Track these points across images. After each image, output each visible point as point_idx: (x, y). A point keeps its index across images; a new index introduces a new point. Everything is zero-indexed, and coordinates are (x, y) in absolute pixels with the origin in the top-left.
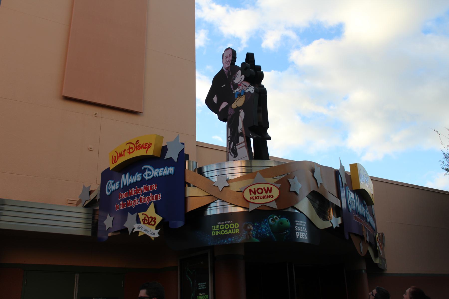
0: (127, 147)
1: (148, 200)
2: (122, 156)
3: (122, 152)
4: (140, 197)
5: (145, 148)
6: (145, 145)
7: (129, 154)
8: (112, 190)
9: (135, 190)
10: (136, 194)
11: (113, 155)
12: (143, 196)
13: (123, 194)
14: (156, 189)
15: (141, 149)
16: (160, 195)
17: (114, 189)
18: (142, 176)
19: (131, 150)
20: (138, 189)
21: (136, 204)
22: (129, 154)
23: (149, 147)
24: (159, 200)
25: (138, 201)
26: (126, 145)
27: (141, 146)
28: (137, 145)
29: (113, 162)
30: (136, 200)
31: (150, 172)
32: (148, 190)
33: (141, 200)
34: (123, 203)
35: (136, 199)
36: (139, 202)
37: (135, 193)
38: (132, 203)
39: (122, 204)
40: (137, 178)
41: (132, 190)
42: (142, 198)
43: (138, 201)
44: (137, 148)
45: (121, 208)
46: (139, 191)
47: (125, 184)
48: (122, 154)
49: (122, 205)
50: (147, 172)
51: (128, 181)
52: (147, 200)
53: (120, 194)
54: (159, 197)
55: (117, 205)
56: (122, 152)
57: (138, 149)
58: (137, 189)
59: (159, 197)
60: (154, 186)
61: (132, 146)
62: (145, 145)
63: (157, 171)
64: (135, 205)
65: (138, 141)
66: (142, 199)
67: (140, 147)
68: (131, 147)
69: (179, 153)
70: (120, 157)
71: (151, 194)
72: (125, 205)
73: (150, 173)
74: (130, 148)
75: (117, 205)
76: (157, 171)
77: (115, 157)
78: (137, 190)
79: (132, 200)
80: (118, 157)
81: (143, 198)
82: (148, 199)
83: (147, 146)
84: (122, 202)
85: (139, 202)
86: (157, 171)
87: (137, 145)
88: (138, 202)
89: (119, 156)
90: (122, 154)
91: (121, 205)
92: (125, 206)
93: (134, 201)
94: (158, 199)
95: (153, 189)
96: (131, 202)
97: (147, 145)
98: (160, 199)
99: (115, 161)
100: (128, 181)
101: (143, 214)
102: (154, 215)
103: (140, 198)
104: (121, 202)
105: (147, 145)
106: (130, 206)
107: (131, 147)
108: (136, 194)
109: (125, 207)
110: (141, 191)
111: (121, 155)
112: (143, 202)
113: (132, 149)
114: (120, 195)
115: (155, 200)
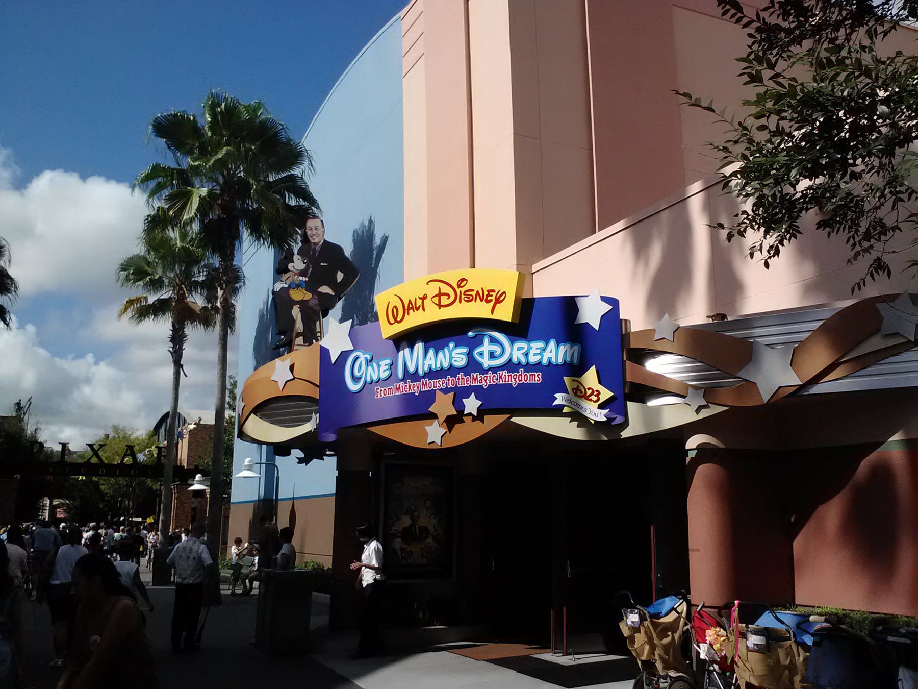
0: (433, 290)
1: (515, 379)
2: (418, 309)
3: (418, 299)
4: (499, 373)
5: (488, 301)
6: (486, 293)
7: (440, 308)
8: (369, 380)
9: (406, 386)
10: (408, 392)
11: (389, 302)
12: (505, 372)
13: (383, 389)
14: (443, 386)
15: (475, 301)
16: (539, 374)
17: (375, 378)
18: (470, 355)
19: (444, 300)
20: (412, 384)
21: (490, 382)
22: (440, 308)
23: (498, 301)
24: (536, 382)
25: (494, 378)
26: (427, 284)
27: (474, 293)
28: (463, 290)
29: (392, 321)
30: (490, 376)
31: (497, 349)
32: (430, 388)
33: (501, 377)
34: (463, 377)
35: (489, 375)
36: (497, 379)
37: (406, 390)
38: (482, 379)
39: (460, 377)
40: (451, 358)
41: (400, 385)
42: (502, 375)
43: (495, 379)
44: (463, 296)
45: (459, 384)
46: (413, 388)
47: (411, 369)
48: (417, 306)
49: (460, 380)
50: (487, 347)
51: (424, 364)
52: (513, 380)
53: (377, 389)
54: (537, 378)
55: (451, 379)
56: (418, 299)
57: (466, 299)
58: (410, 384)
59: (537, 378)
60: (441, 383)
61: (445, 289)
62: (486, 293)
63: (523, 348)
64: (488, 383)
65: (463, 280)
66: (503, 376)
67: (472, 295)
68: (442, 292)
69: (602, 316)
70: (411, 311)
71: (521, 371)
72: (467, 381)
73: (496, 351)
74: (440, 295)
75: (451, 379)
76: (523, 348)
77: (395, 309)
78: (410, 387)
79: (482, 375)
80: (406, 311)
81: (505, 375)
82: (516, 378)
83: (493, 298)
84: (461, 375)
85: (497, 379)
86: (519, 349)
87: (463, 290)
88: (494, 380)
89: (409, 309)
90: (417, 306)
91: (459, 379)
92: (468, 382)
93: (487, 377)
94: (535, 381)
95: (439, 387)
96: (479, 379)
97: (494, 294)
98: (539, 381)
99: (395, 319)
100: (424, 364)
101: (573, 380)
102: (596, 386)
103: (498, 374)
104: (460, 376)
105: (494, 294)
106: (479, 384)
107: (442, 292)
108: (409, 391)
109: (467, 384)
110: (418, 388)
111: (411, 307)
112: (505, 381)
113: (447, 297)
114: (378, 391)
115: (530, 381)
